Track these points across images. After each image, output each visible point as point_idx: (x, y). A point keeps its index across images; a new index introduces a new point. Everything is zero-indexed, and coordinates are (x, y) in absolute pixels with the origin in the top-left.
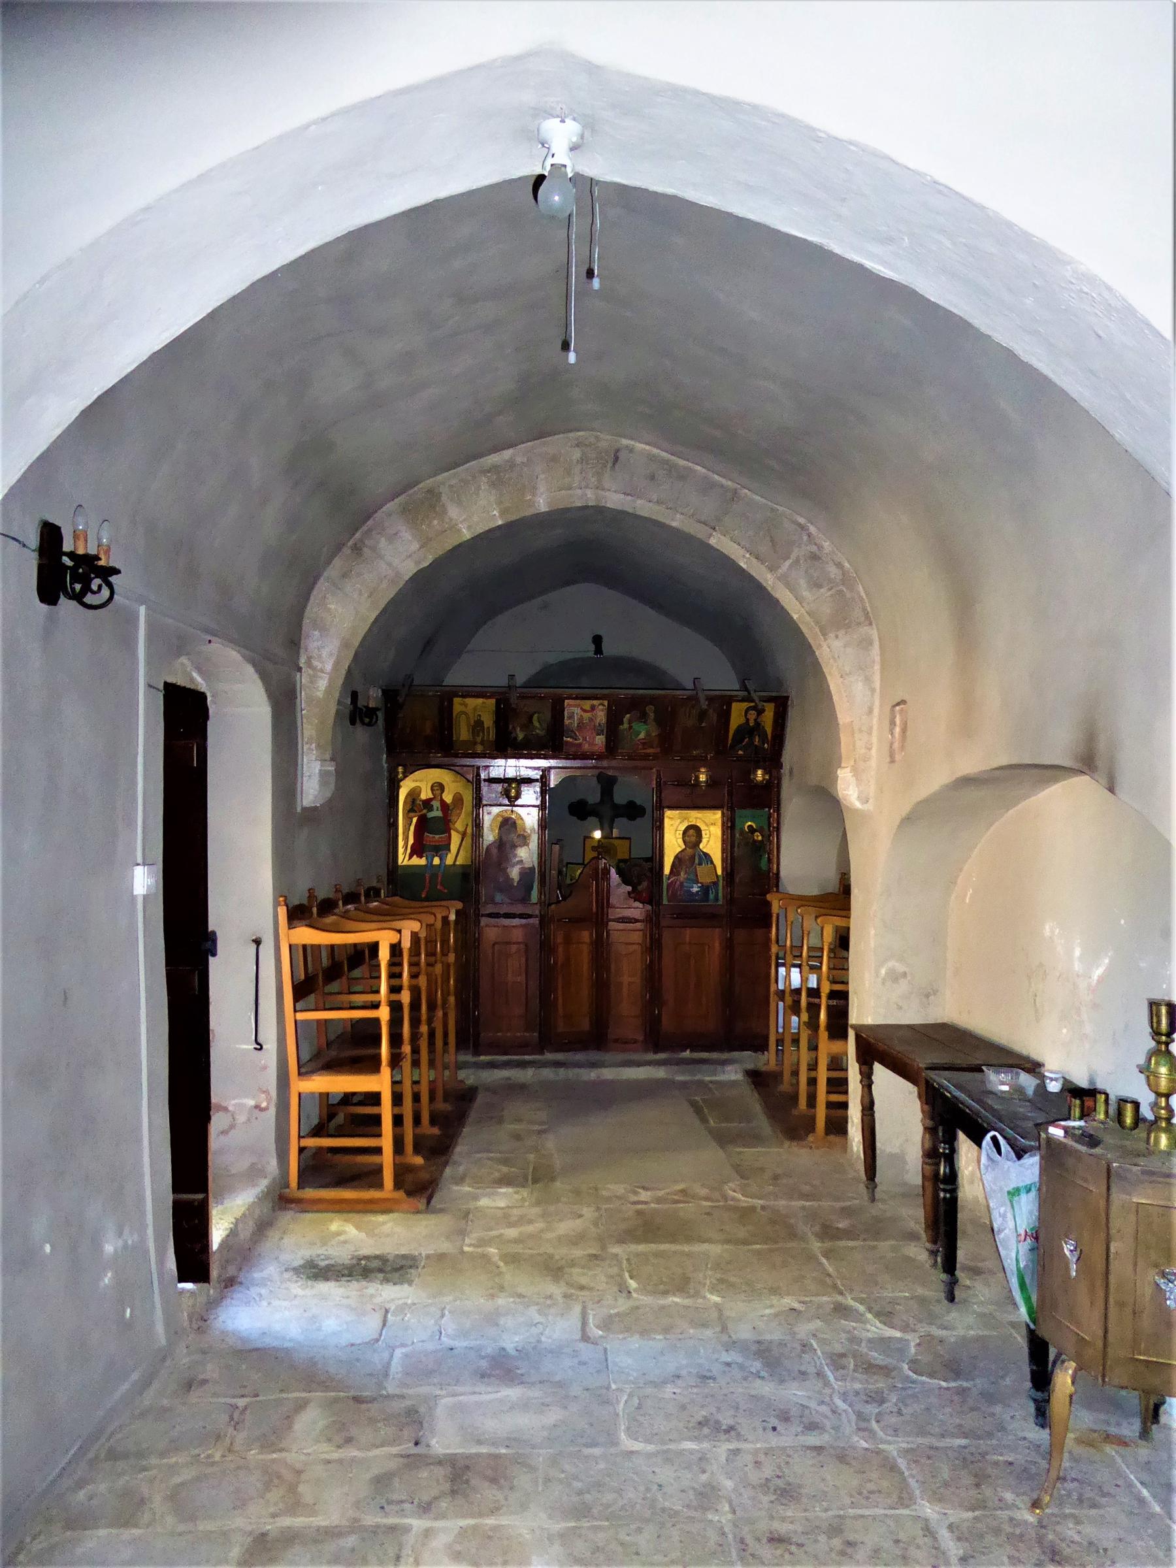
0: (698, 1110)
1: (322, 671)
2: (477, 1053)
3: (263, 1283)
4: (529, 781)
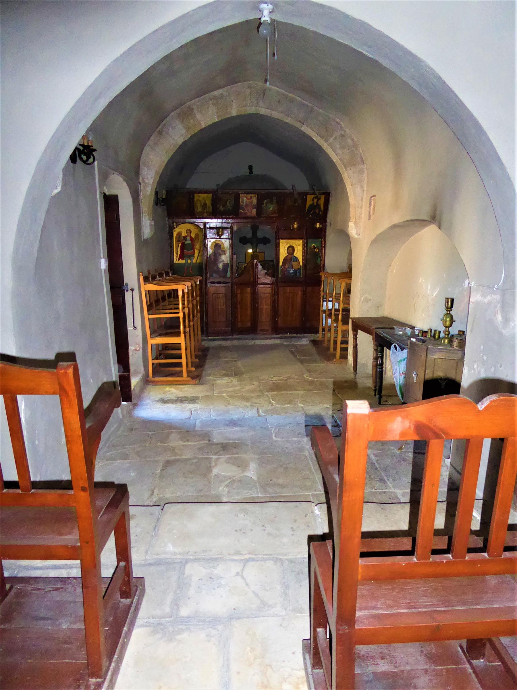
0: (292, 353)
1: (148, 183)
2: (207, 336)
3: (146, 405)
4: (226, 228)
